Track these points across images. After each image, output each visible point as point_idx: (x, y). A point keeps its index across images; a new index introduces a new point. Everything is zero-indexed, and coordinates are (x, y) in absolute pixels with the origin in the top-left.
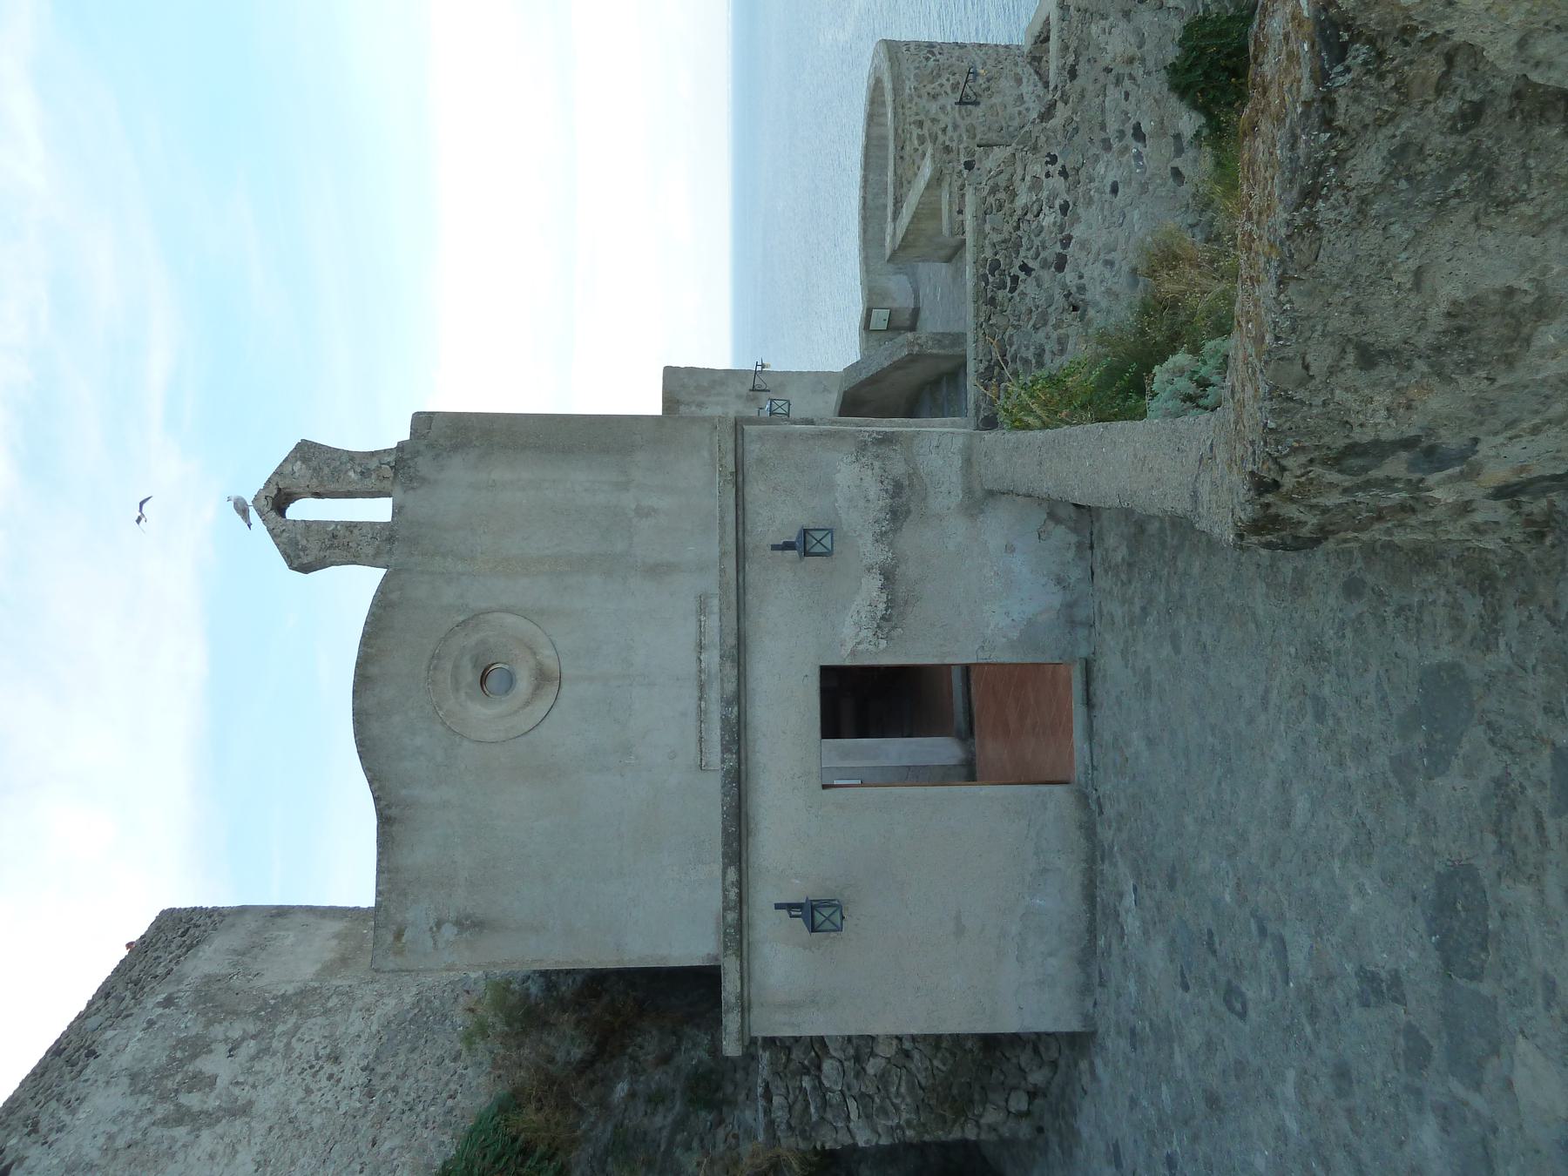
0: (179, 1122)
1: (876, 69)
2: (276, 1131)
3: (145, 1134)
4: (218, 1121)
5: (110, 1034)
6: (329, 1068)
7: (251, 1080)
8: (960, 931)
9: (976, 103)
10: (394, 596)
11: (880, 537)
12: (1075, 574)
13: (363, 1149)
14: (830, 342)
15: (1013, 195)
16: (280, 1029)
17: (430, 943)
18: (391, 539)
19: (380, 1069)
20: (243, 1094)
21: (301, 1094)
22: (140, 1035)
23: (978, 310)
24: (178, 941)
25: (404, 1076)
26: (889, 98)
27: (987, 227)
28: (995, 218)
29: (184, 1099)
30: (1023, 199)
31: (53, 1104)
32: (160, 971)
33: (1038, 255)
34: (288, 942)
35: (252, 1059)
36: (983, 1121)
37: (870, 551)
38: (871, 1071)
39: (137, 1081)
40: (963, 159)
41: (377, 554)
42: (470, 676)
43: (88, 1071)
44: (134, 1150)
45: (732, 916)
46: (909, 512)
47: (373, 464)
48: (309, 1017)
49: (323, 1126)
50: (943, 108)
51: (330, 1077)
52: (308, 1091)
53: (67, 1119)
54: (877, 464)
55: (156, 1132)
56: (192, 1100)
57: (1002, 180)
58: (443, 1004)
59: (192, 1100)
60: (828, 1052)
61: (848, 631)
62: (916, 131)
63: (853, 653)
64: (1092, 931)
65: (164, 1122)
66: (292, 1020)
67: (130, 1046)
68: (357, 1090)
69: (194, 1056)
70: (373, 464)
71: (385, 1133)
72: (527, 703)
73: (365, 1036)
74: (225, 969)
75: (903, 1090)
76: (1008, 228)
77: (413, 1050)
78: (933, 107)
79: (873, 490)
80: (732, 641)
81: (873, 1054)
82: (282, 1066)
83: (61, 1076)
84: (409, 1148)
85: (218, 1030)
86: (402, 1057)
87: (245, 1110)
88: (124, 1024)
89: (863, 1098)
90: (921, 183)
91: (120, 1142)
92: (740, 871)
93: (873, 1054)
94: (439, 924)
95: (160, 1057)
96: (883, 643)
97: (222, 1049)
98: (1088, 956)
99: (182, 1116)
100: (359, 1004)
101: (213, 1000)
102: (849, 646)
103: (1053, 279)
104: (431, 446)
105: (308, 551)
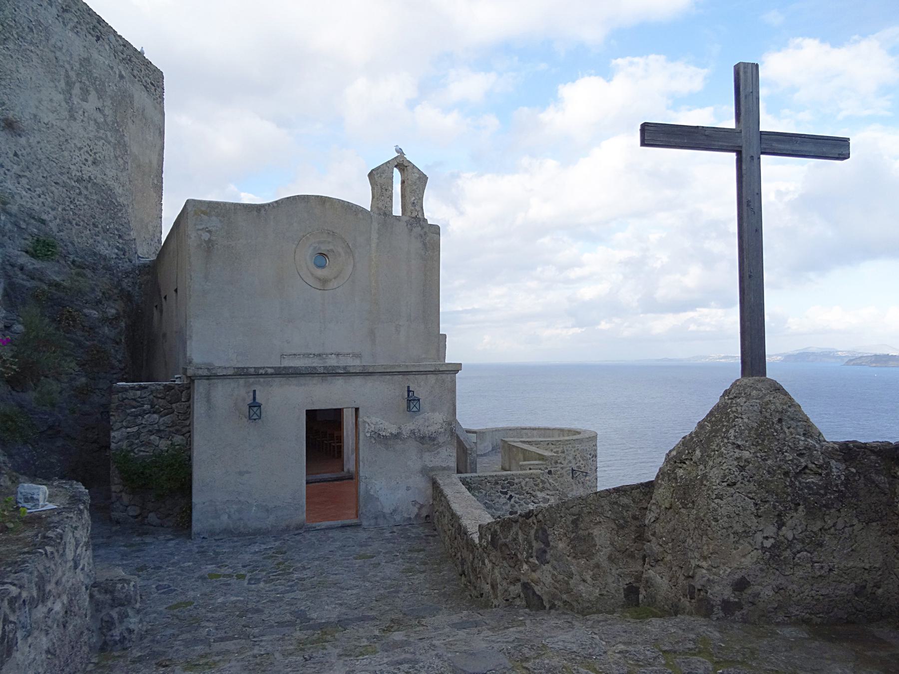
0: (67, 83)
1: (585, 431)
2: (62, 133)
3: (61, 66)
4: (67, 103)
5: (107, 47)
6: (90, 159)
7: (85, 119)
8: (241, 473)
9: (573, 477)
10: (360, 216)
11: (413, 432)
12: (398, 518)
13: (53, 177)
14: (474, 413)
15: (541, 491)
16: (109, 134)
17: (201, 227)
18: (385, 214)
19: (89, 185)
20: (79, 115)
21: (79, 145)
22: (107, 63)
23: (493, 476)
24: (149, 81)
25: (86, 198)
26: (571, 438)
27: (527, 480)
28: (531, 483)
29: (77, 85)
30: (540, 495)
31: (76, 20)
32: (135, 72)
33: (516, 502)
34: (148, 136)
35: (95, 120)
36: (123, 494)
37: (408, 427)
38: (152, 437)
39: (86, 61)
40: (552, 470)
41: (375, 210)
42: (324, 248)
43: (90, 37)
44: (54, 61)
45: (252, 371)
46: (423, 444)
47: (418, 208)
48: (115, 149)
49: (64, 157)
50: (570, 462)
51: (86, 160)
52: (80, 149)
53: (69, 27)
54: (442, 430)
55: (63, 73)
56: (76, 91)
57: (547, 485)
58: (119, 218)
59: (76, 91)
60: (161, 416)
61: (374, 419)
62: (560, 450)
63: (365, 422)
64: (240, 534)
65: (67, 76)
66: (113, 140)
67: (102, 58)
68: (79, 174)
69: (96, 90)
70: (418, 208)
71: (60, 189)
72: (312, 274)
73: (105, 177)
74: (136, 105)
75: (142, 453)
76: (527, 489)
77: (98, 202)
78: (571, 458)
79: (432, 429)
80: (371, 370)
81: (161, 438)
82: (91, 135)
83: (88, 23)
84: (53, 202)
85: (108, 102)
86: (95, 197)
87: (73, 117)
88: (112, 55)
89: (138, 433)
90: (540, 452)
91: (58, 54)
92: (272, 374)
93: (161, 438)
94: (209, 232)
95: (96, 73)
96: (368, 435)
97: (100, 105)
98: (230, 533)
99: (69, 84)
100: (119, 174)
101: (123, 101)
102: (367, 420)
103: (507, 511)
104: (425, 233)
105: (378, 178)
